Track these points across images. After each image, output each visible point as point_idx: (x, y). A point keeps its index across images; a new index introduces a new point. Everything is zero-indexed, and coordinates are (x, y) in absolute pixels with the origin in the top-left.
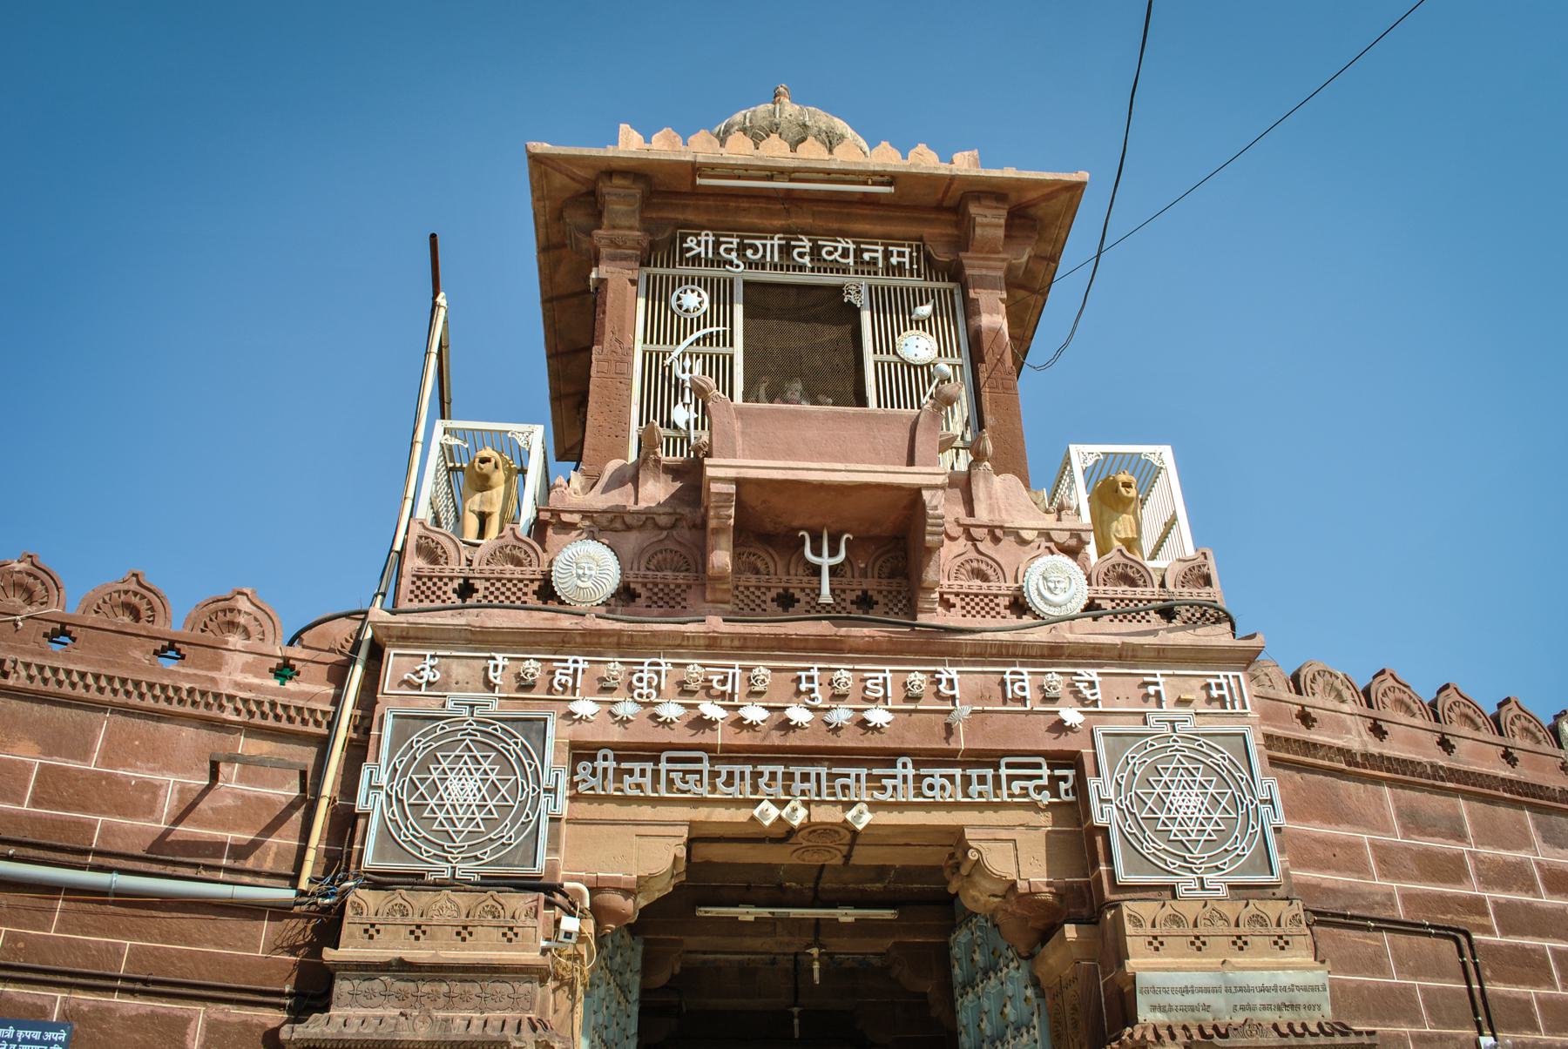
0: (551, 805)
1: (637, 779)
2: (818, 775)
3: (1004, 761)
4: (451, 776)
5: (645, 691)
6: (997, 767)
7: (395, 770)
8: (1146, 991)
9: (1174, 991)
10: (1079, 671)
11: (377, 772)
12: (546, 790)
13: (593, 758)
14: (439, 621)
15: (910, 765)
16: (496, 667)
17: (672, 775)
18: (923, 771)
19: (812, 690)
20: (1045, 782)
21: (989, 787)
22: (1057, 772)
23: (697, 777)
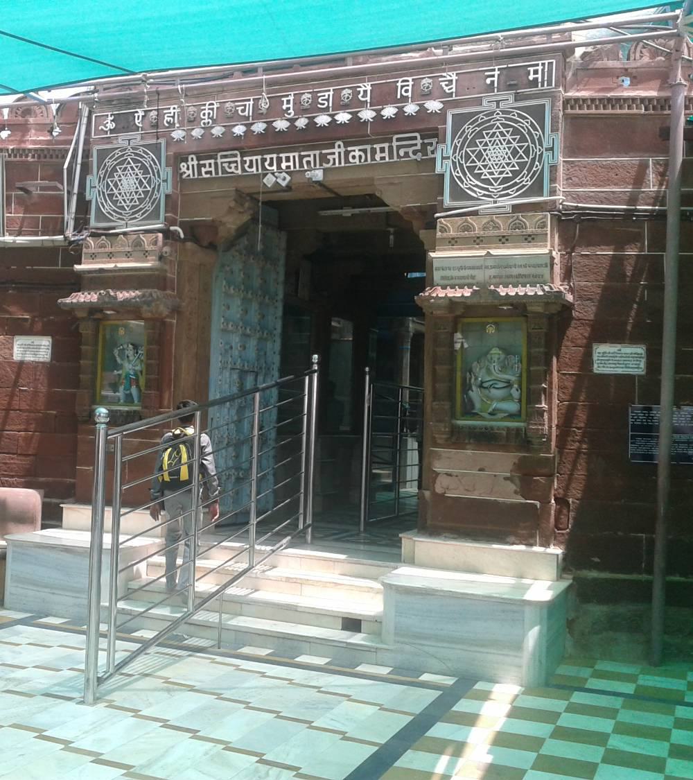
0: (551, 157)
1: (208, 169)
2: (294, 157)
3: (219, 154)
4: (123, 177)
5: (206, 121)
6: (390, 141)
7: (456, 146)
8: (438, 269)
9: (454, 269)
10: (444, 74)
11: (92, 179)
12: (448, 158)
13: (186, 160)
14: (110, 94)
15: (195, 159)
16: (139, 117)
17: (224, 165)
18: (349, 149)
19: (289, 109)
20: (419, 147)
21: (386, 154)
22: (426, 141)
23: (235, 165)
